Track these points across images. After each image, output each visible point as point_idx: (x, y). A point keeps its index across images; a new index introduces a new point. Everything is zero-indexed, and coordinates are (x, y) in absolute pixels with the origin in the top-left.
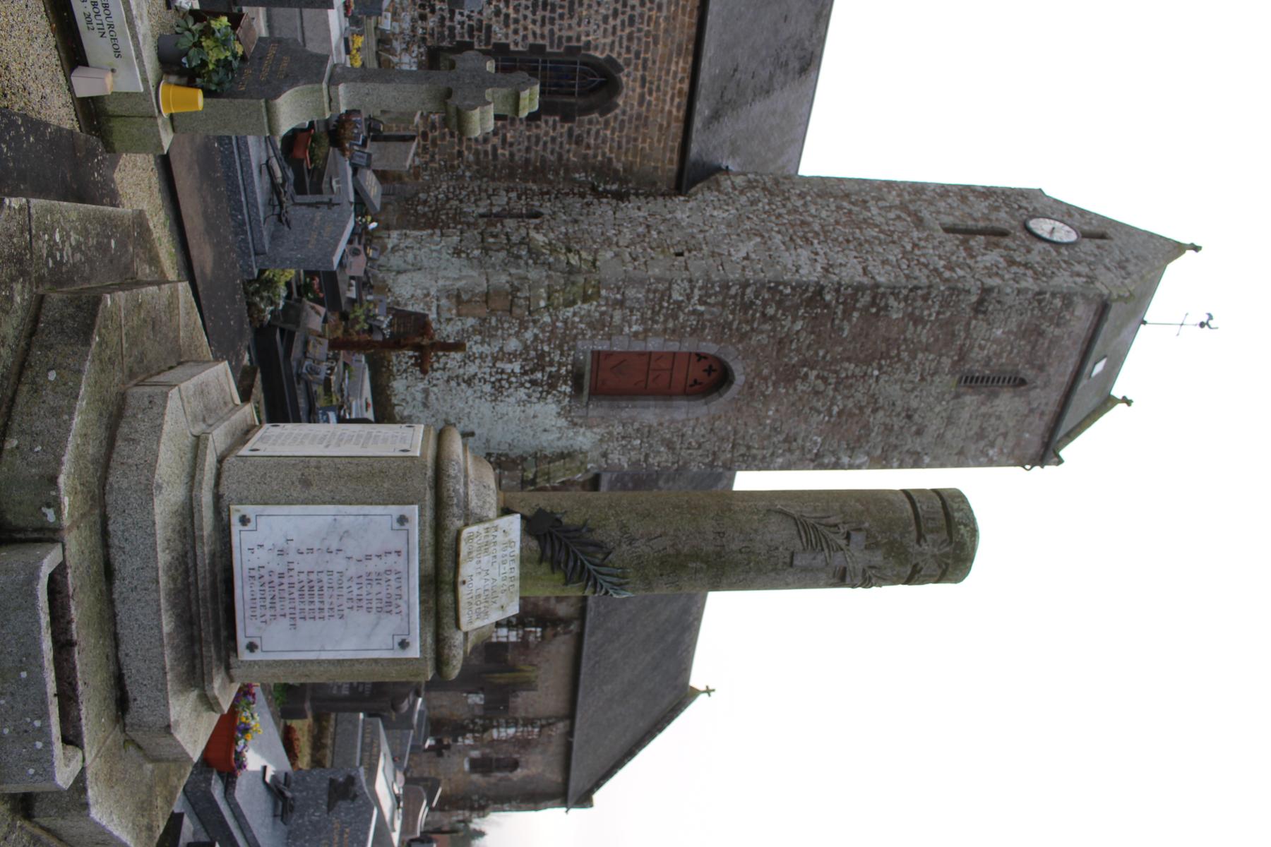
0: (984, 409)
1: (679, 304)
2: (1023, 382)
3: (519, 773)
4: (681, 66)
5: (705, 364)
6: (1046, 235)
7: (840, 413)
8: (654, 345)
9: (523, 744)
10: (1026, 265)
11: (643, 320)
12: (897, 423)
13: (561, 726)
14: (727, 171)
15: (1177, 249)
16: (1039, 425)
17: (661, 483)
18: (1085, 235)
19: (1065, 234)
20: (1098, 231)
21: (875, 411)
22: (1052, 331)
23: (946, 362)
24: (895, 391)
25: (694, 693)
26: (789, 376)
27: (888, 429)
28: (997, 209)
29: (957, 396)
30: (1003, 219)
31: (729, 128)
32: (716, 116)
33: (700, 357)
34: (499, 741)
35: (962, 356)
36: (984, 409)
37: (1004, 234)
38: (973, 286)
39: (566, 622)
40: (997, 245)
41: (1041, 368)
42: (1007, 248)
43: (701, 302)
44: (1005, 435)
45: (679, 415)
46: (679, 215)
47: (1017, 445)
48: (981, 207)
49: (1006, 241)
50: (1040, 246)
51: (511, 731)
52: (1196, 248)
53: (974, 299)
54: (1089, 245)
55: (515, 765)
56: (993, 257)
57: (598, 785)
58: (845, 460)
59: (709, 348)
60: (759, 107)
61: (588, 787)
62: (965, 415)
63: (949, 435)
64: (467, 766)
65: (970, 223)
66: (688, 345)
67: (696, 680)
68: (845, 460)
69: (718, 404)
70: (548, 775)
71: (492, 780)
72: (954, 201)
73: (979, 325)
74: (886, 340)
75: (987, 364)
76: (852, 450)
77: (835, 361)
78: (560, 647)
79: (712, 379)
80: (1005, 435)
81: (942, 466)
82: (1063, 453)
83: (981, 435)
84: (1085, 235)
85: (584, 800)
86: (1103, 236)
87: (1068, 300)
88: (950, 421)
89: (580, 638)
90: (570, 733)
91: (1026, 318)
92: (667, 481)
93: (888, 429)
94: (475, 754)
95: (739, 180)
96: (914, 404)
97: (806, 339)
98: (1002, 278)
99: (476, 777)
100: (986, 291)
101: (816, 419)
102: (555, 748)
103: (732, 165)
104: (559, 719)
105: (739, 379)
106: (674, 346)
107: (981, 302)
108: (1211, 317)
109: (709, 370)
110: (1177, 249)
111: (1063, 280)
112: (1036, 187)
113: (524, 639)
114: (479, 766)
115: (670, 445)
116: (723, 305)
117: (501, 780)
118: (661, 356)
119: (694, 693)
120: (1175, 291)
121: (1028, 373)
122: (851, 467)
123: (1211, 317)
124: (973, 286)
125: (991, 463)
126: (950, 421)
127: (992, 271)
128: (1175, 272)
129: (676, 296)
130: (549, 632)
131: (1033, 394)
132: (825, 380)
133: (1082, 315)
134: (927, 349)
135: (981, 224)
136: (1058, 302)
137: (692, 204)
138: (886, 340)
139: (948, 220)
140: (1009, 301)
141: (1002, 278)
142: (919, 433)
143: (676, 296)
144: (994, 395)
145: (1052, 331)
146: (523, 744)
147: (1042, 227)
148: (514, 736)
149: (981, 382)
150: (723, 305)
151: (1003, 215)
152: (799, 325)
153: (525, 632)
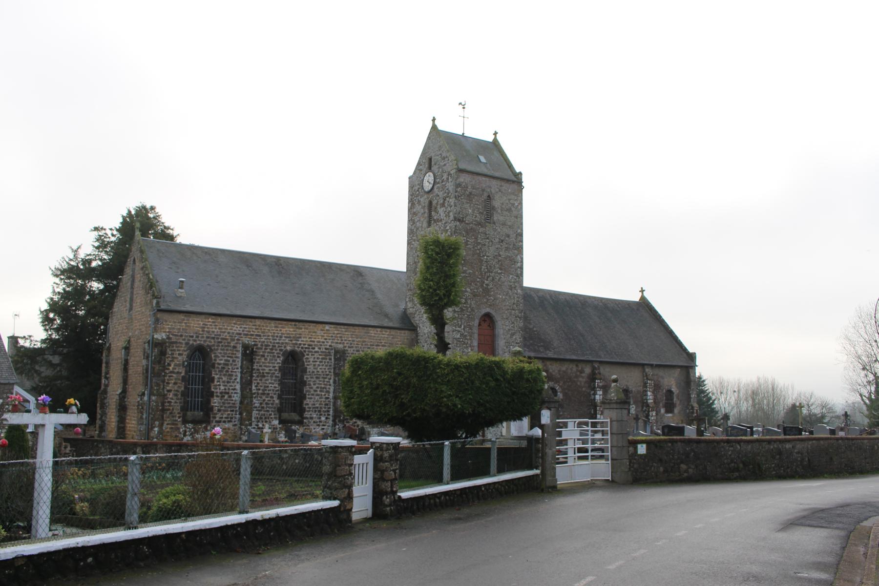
0: (499, 211)
1: (461, 335)
2: (489, 196)
3: (674, 389)
4: (372, 332)
5: (482, 323)
6: (431, 186)
7: (501, 269)
8: (475, 343)
9: (657, 387)
10: (445, 200)
11: (467, 348)
12: (504, 245)
13: (648, 370)
14: (405, 309)
15: (434, 127)
16: (505, 186)
17: (531, 327)
18: (430, 168)
19: (429, 178)
20: (427, 162)
21: (500, 256)
22: (469, 189)
23: (481, 230)
24: (492, 249)
25: (643, 298)
26: (487, 291)
27: (507, 249)
28: (419, 202)
29: (494, 223)
30: (424, 200)
31: (390, 310)
32: (386, 316)
33: (480, 325)
34: (655, 399)
35: (479, 224)
36: (499, 211)
37: (430, 203)
38: (453, 224)
39: (594, 369)
40: (436, 208)
41: (483, 190)
42: (437, 204)
43: (460, 327)
44: (509, 200)
45: (501, 332)
46: (426, 331)
47: (513, 194)
48: (418, 208)
49: (434, 202)
50: (435, 189)
51: (649, 393)
52: (434, 120)
53: (458, 223)
54: (434, 168)
55: (670, 392)
56: (441, 211)
57: (685, 350)
58: (519, 264)
59: (477, 322)
60: (379, 296)
61: (685, 355)
62: (501, 218)
63: (509, 224)
64: (670, 415)
65: (426, 215)
66: (476, 330)
67: (636, 298)
68: (519, 264)
69: (497, 317)
70: (676, 375)
71: (678, 402)
72: (416, 219)
73: (468, 219)
74: (473, 255)
75: (482, 213)
76: (515, 262)
77: (481, 274)
78: (605, 370)
79: (488, 319)
80: (509, 200)
81: (522, 224)
82: (518, 171)
83: (509, 210)
84: (430, 168)
85: (692, 357)
86: (430, 159)
87: (458, 185)
88: (504, 224)
89: (601, 362)
90: (652, 365)
91: (465, 201)
92: (530, 324)
93: (507, 249)
94: (663, 411)
95: (410, 305)
96: (497, 240)
97: (473, 286)
98: (450, 212)
99: (676, 411)
100: (455, 219)
101: (503, 279)
102: (661, 372)
103: (403, 307)
104: (644, 371)
105: (488, 310)
106: (476, 336)
107: (459, 220)
108: (460, 104)
109: (485, 321)
110: (434, 127)
111: (450, 186)
112: (408, 180)
113: (601, 388)
114: (670, 408)
115: (513, 335)
116: (461, 319)
117: (678, 398)
118: (479, 339)
119: (643, 298)
120: (450, 125)
121: (486, 194)
122: (522, 262)
123: (460, 104)
124: (453, 224)
125: (521, 203)
126: (504, 224)
127: (448, 216)
128: (441, 127)
129: (458, 336)
130: (598, 376)
131: (493, 191)
132: (488, 277)
133: (464, 179)
134: (476, 238)
135: (427, 211)
136: (459, 189)
137: (421, 325)
138: (473, 255)
139: (425, 224)
140: (458, 209)
141: (450, 212)
142: (508, 236)
143: (458, 336)
144: (494, 208)
145: (469, 189)
146: (657, 387)
147: (427, 186)
148: (653, 392)
149: (489, 211)
150: (461, 319)
151: (422, 200)
152: (468, 290)
153: (84, 435)
